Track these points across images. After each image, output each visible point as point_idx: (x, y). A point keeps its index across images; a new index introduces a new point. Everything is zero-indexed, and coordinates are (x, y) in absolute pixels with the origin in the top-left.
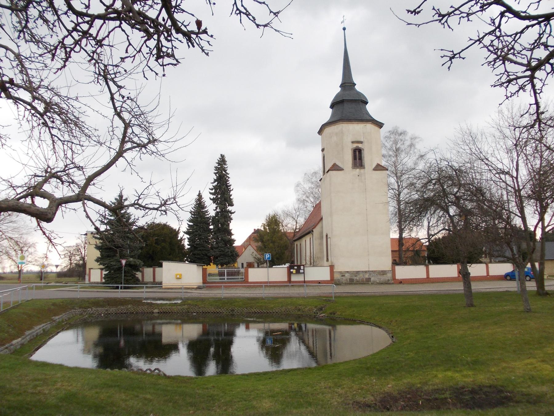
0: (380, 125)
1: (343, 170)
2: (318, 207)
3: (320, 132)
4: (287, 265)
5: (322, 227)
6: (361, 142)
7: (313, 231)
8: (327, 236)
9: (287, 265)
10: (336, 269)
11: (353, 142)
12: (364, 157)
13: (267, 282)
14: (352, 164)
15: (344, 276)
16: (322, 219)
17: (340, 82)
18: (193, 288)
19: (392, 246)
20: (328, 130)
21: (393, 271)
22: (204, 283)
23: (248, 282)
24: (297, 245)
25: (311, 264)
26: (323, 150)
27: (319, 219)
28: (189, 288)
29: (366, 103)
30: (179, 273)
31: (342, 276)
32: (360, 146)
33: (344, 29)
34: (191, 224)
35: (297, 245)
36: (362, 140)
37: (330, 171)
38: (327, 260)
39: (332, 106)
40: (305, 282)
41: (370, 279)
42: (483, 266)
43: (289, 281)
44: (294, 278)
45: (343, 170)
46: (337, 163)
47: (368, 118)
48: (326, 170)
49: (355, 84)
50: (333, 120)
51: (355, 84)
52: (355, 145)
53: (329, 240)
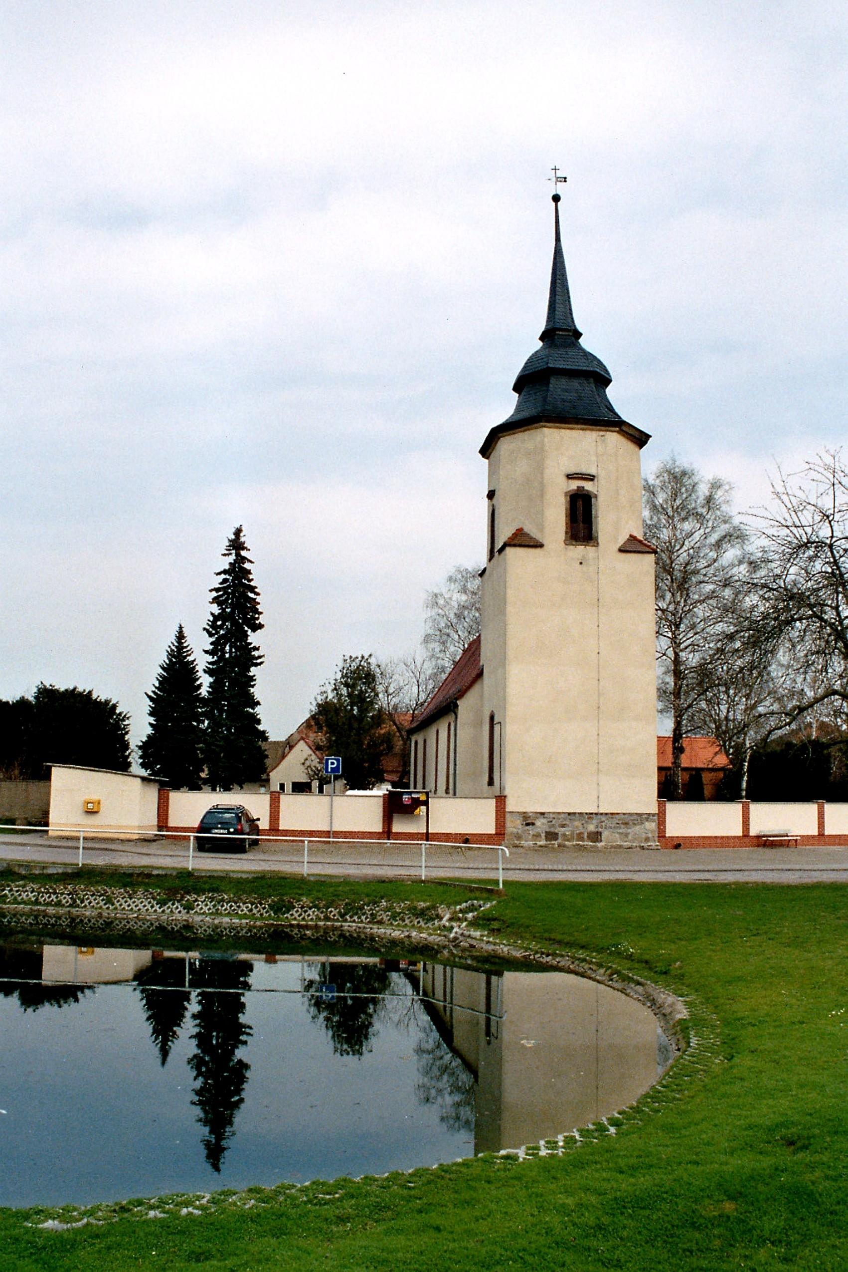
0: (640, 439)
1: (541, 546)
2: (473, 650)
3: (486, 450)
4: (382, 790)
5: (482, 696)
6: (591, 478)
7: (456, 706)
8: (492, 718)
9: (382, 790)
10: (511, 806)
11: (570, 477)
12: (597, 517)
13: (329, 832)
14: (566, 533)
15: (533, 824)
16: (480, 675)
17: (541, 325)
18: (129, 841)
19: (661, 753)
20: (505, 445)
21: (661, 817)
22: (160, 828)
23: (278, 830)
24: (416, 743)
25: (447, 792)
26: (491, 495)
27: (474, 673)
28: (112, 840)
29: (607, 381)
30: (95, 797)
31: (528, 824)
32: (588, 486)
33: (556, 198)
34: (210, 690)
35: (416, 743)
36: (592, 471)
37: (508, 550)
38: (491, 782)
39: (517, 388)
40: (427, 836)
41: (601, 833)
42: (811, 809)
43: (388, 833)
44: (397, 828)
45: (541, 546)
46: (526, 529)
47: (610, 417)
48: (499, 545)
49: (581, 334)
50: (525, 414)
51: (581, 334)
52: (574, 485)
53: (497, 728)
